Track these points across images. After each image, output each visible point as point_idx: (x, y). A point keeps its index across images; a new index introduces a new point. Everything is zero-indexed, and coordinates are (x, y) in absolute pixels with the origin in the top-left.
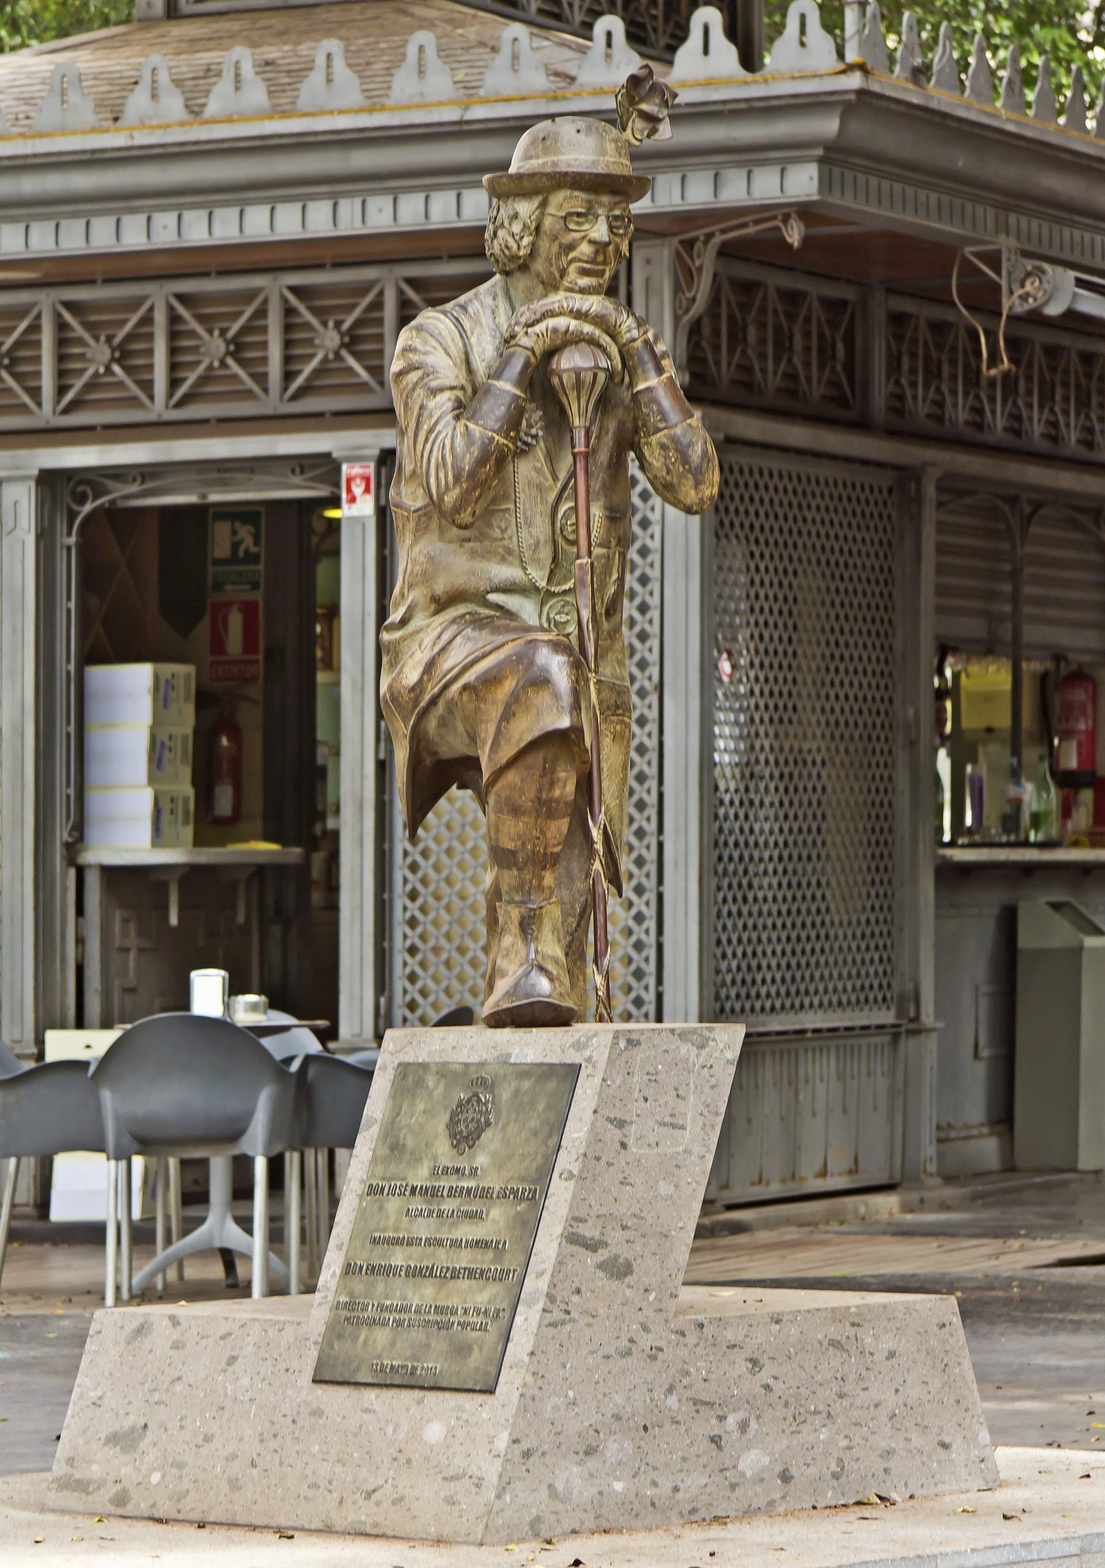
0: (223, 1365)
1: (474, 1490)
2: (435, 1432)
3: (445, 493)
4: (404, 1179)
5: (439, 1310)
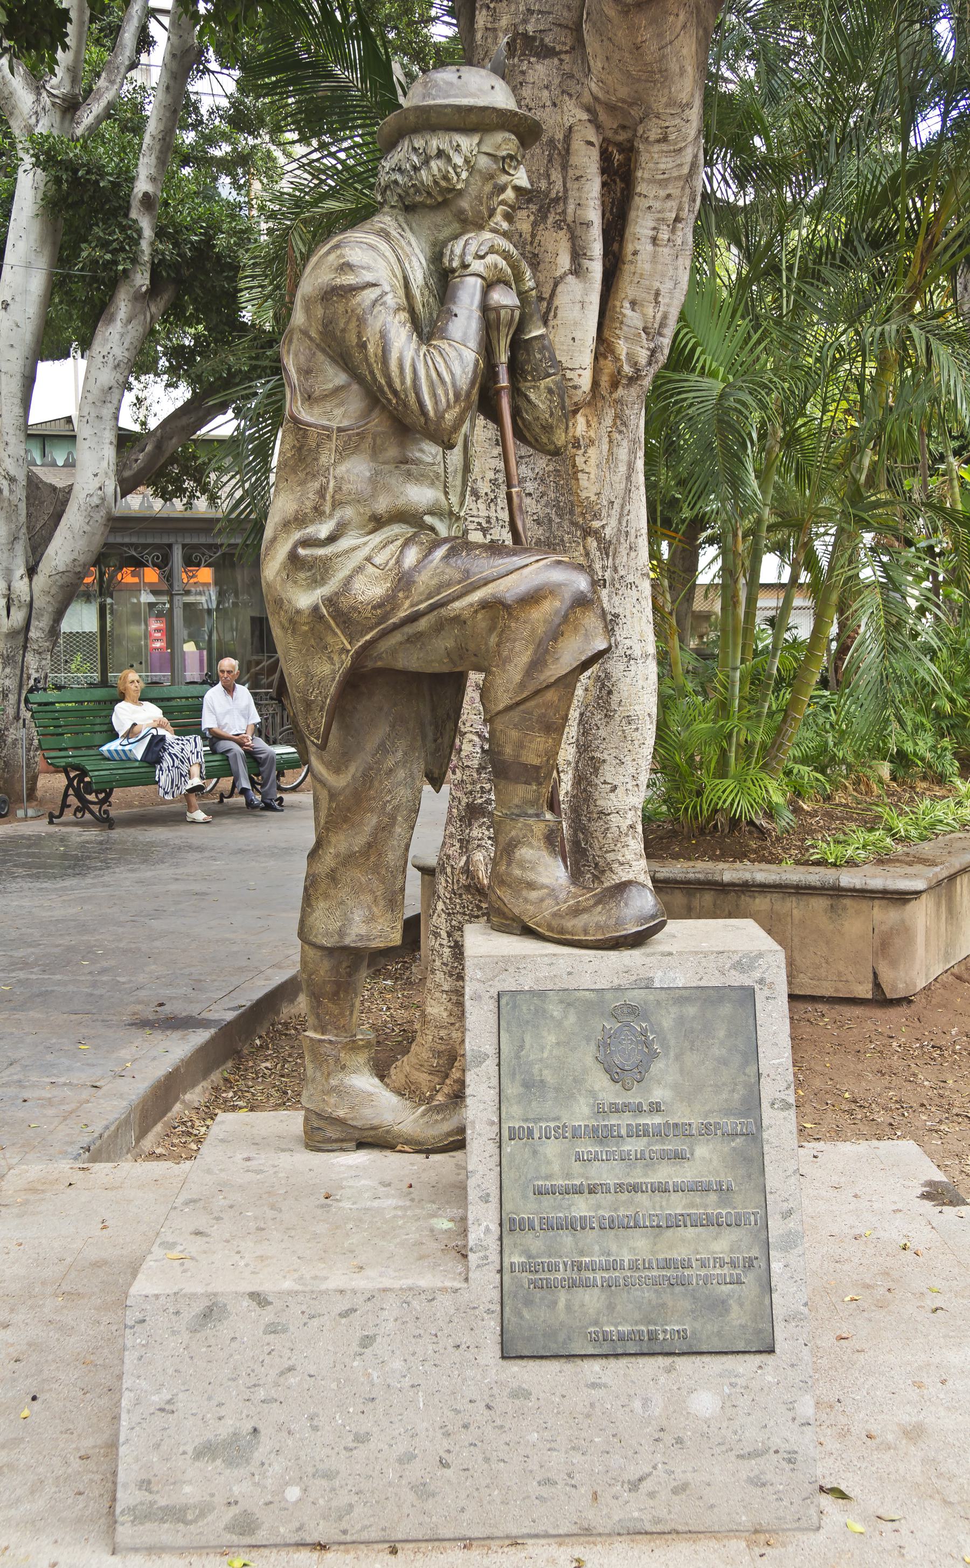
0: (355, 1348)
1: (787, 1467)
2: (705, 1403)
3: (445, 411)
4: (557, 1119)
5: (668, 1264)
